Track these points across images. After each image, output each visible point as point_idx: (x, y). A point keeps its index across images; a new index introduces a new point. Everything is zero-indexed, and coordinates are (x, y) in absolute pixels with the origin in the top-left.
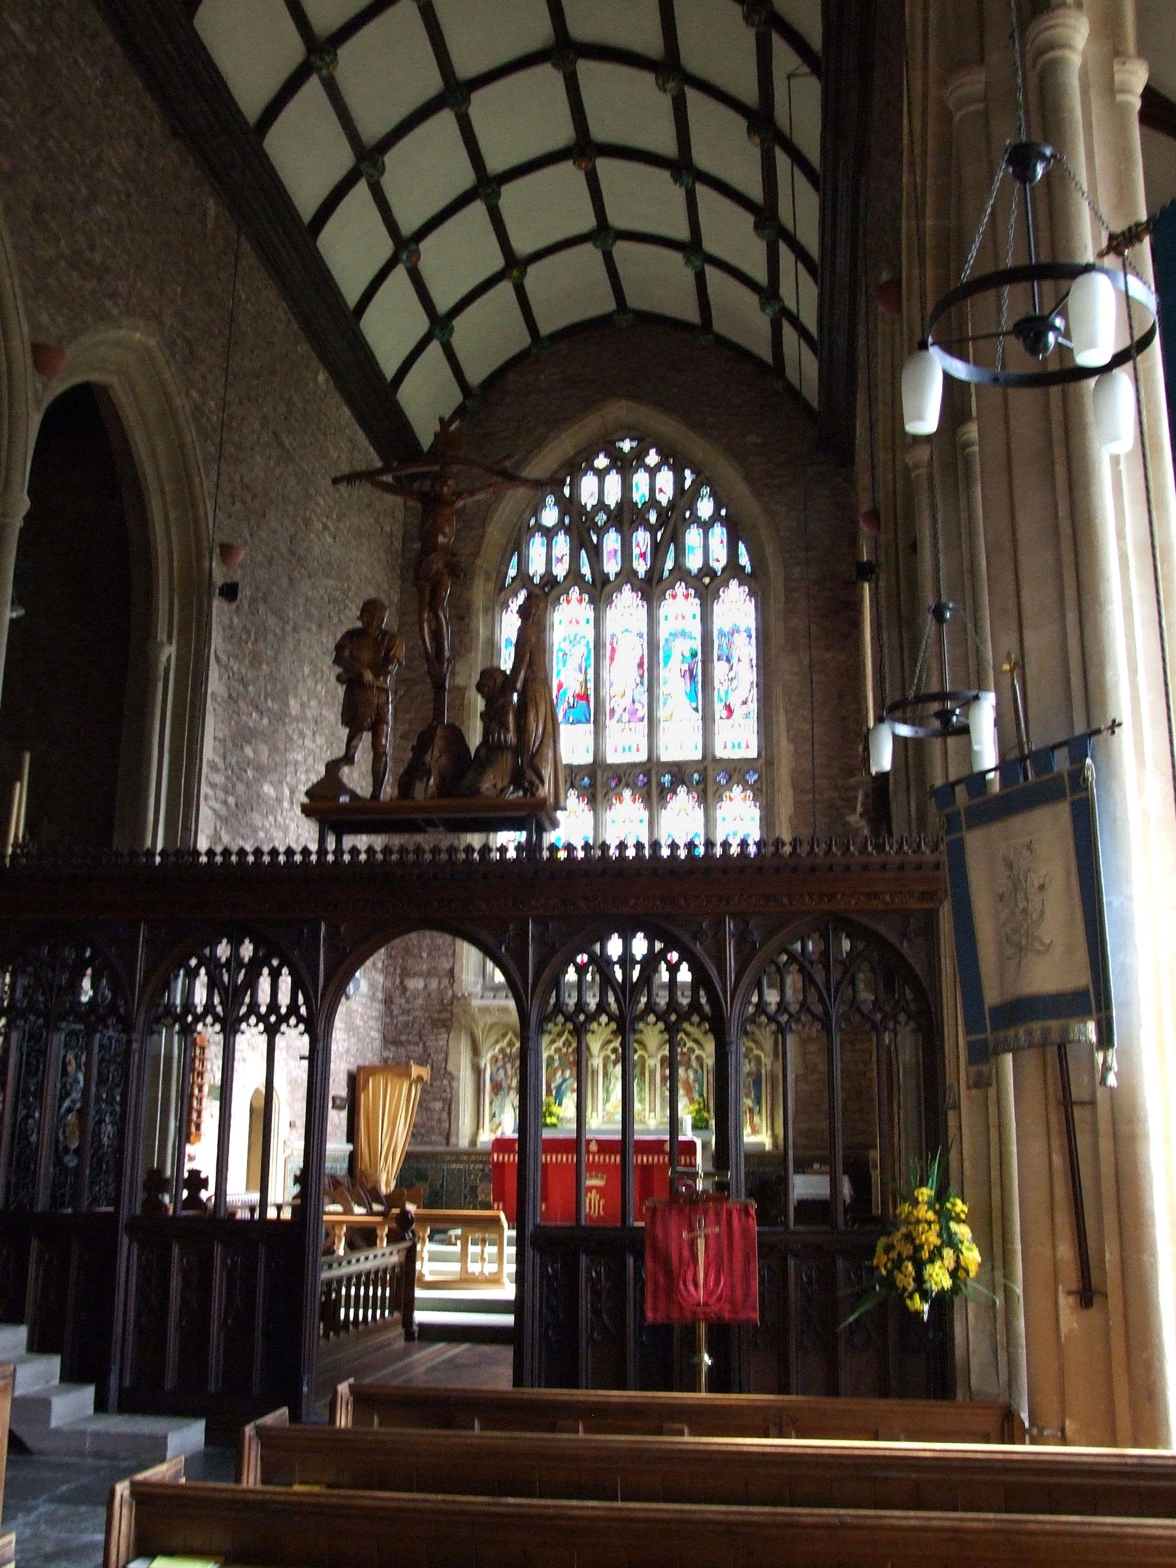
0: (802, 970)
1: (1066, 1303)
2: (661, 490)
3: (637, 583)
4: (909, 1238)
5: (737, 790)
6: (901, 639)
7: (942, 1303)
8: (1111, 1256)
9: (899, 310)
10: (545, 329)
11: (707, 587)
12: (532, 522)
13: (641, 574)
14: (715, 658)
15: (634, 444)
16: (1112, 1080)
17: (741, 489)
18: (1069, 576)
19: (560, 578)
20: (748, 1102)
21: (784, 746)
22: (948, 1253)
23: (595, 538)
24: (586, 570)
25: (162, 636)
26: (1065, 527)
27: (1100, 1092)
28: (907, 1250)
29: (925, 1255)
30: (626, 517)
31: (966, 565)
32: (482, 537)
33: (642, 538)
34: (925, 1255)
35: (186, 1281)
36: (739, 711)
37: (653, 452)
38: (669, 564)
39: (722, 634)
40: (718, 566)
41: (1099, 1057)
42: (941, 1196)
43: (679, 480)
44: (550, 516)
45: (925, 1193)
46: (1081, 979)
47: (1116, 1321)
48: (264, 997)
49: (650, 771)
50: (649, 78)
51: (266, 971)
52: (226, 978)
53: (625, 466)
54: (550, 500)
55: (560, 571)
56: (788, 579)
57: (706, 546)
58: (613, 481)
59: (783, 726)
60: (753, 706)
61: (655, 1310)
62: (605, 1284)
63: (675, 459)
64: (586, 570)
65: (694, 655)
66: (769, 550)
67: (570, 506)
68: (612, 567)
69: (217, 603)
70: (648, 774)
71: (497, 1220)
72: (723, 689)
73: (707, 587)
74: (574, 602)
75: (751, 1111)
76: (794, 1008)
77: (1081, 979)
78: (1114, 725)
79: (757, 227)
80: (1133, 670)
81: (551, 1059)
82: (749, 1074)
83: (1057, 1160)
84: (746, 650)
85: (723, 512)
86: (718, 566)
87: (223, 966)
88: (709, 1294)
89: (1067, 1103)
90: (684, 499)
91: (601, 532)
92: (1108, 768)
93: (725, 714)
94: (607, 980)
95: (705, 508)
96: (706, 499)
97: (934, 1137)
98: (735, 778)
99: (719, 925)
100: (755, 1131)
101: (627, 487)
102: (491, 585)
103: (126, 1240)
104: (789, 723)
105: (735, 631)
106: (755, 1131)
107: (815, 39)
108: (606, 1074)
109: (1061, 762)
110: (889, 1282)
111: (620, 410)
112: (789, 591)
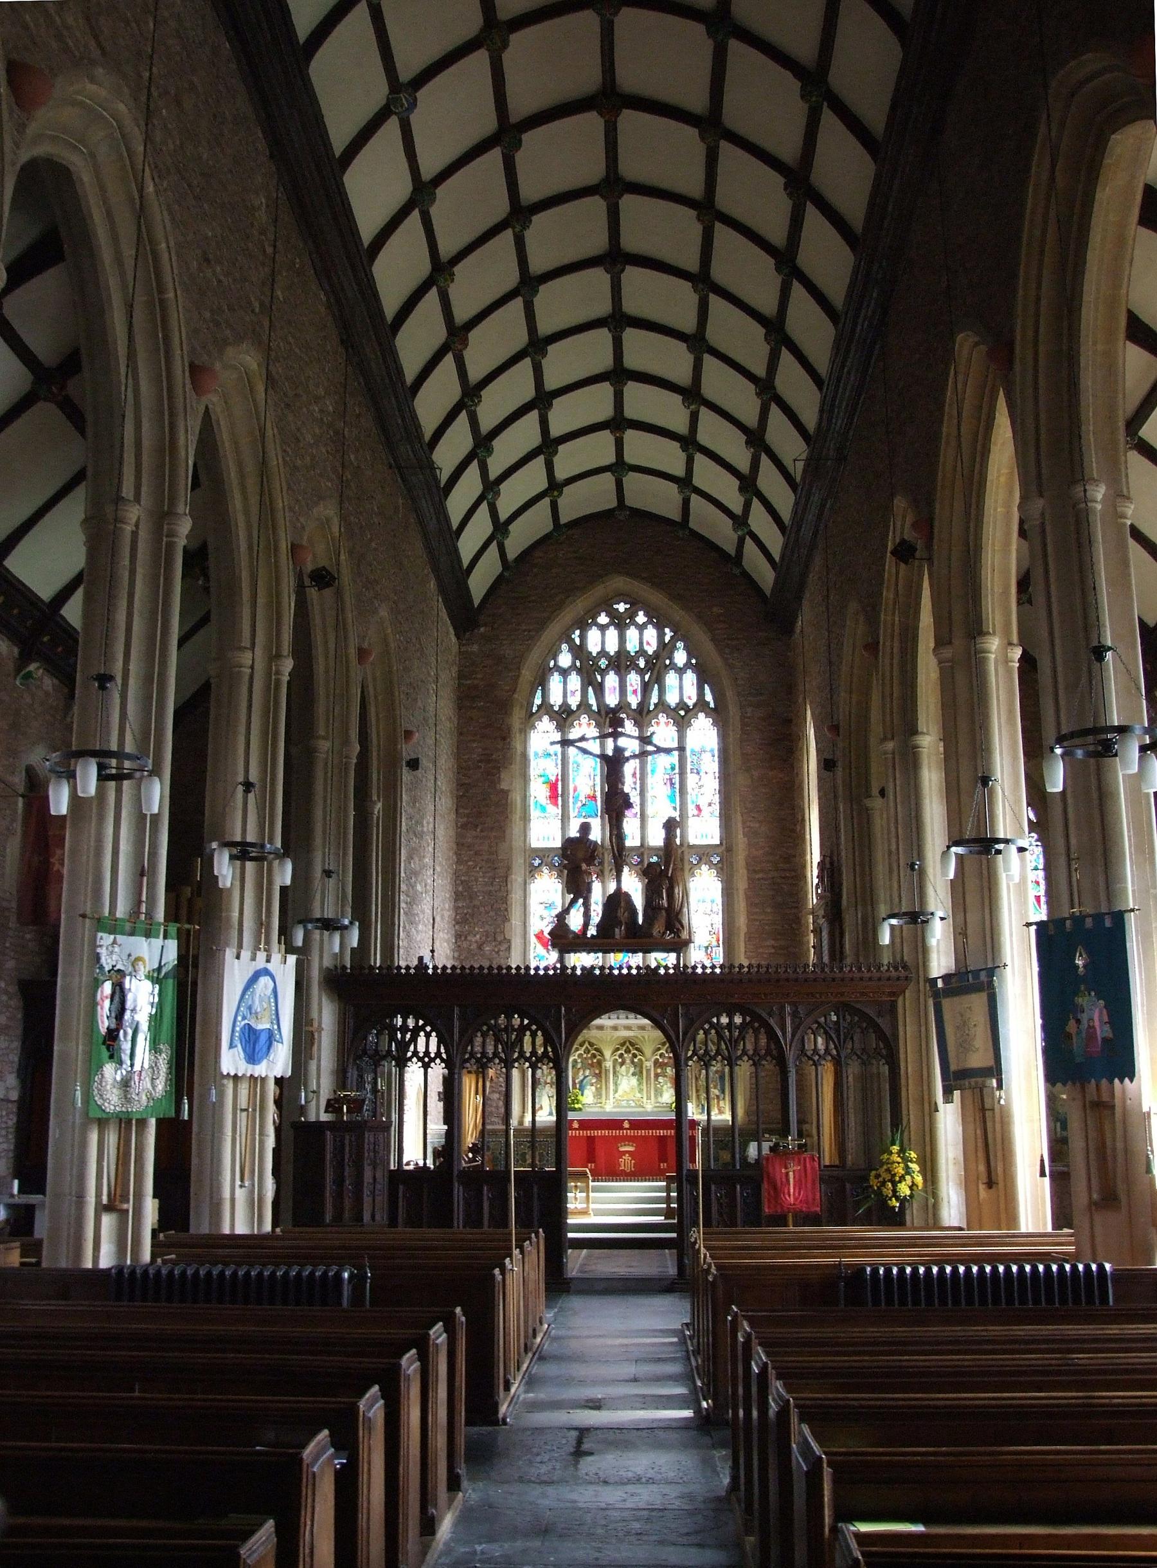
0: (826, 1032)
1: (982, 1187)
2: (648, 643)
3: (631, 713)
4: (888, 1171)
5: (705, 868)
6: (852, 811)
7: (903, 1201)
8: (1000, 1170)
9: (876, 657)
10: (564, 520)
11: (682, 716)
12: (552, 664)
13: (634, 706)
14: (689, 771)
15: (628, 606)
16: (1002, 1102)
17: (709, 647)
18: (986, 891)
19: (574, 708)
20: (717, 1092)
21: (741, 841)
22: (908, 1177)
23: (599, 678)
24: (592, 701)
25: (375, 798)
26: (985, 872)
27: (996, 1106)
28: (888, 1177)
29: (897, 1179)
30: (621, 662)
31: (913, 814)
32: (519, 676)
33: (633, 679)
34: (897, 1179)
35: (491, 1206)
36: (706, 810)
37: (641, 613)
38: (654, 699)
39: (693, 753)
40: (691, 703)
41: (997, 1093)
42: (902, 1151)
43: (661, 636)
44: (565, 659)
45: (895, 1148)
46: (991, 1062)
47: (1002, 1193)
48: (528, 1048)
49: (642, 854)
50: (678, 398)
51: (528, 1033)
52: (399, 1036)
53: (621, 623)
54: (564, 647)
55: (574, 702)
56: (743, 717)
57: (681, 686)
58: (612, 634)
59: (740, 825)
60: (716, 808)
61: (769, 1207)
62: (724, 1200)
63: (659, 620)
64: (592, 701)
65: (673, 769)
66: (729, 694)
67: (579, 651)
68: (612, 700)
69: (405, 769)
70: (641, 855)
71: (585, 1174)
72: (694, 793)
73: (682, 716)
74: (584, 726)
75: (718, 1097)
76: (822, 1052)
77: (991, 1062)
78: (1005, 965)
79: (741, 489)
80: (1011, 935)
81: (575, 1061)
82: (717, 1072)
83: (978, 1132)
84: (711, 766)
85: (694, 661)
86: (691, 703)
87: (502, 1030)
88: (796, 1199)
89: (983, 1109)
90: (665, 649)
91: (603, 672)
92: (1002, 980)
93: (696, 812)
94: (720, 1037)
95: (680, 657)
96: (681, 651)
97: (896, 1121)
98: (704, 860)
99: (782, 1008)
100: (721, 1112)
101: (622, 640)
102: (523, 713)
103: (456, 1185)
104: (744, 823)
105: (703, 751)
106: (721, 1112)
107: (822, 365)
108: (614, 1073)
109: (983, 976)
110: (879, 1193)
111: (619, 582)
112: (744, 725)
